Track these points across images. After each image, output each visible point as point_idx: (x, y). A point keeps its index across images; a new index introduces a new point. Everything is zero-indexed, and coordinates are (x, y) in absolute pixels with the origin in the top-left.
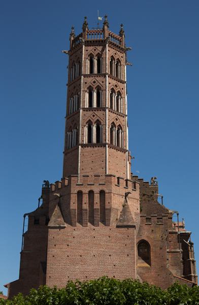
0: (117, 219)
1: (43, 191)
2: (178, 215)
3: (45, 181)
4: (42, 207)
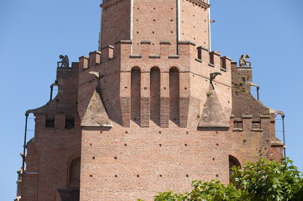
0: (199, 117)
1: (58, 72)
2: (283, 117)
3: (61, 57)
4: (57, 100)
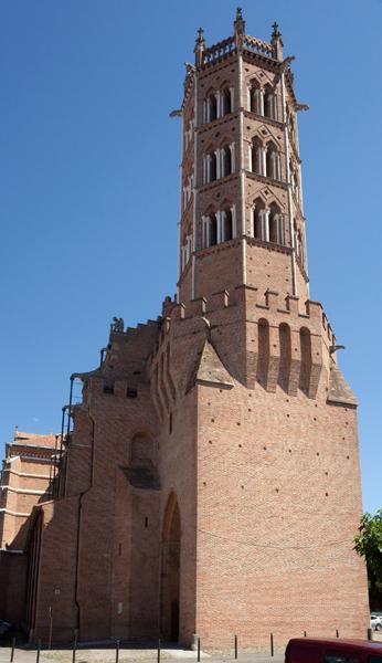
3: (115, 319)
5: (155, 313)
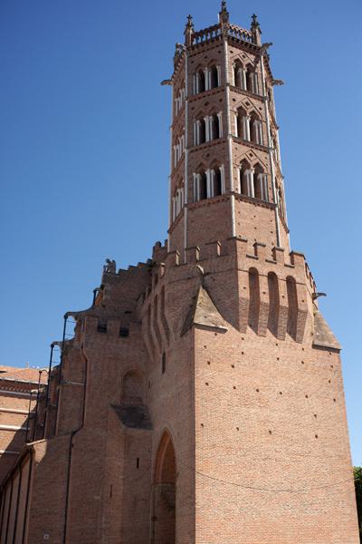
3: (108, 261)
5: (146, 255)
